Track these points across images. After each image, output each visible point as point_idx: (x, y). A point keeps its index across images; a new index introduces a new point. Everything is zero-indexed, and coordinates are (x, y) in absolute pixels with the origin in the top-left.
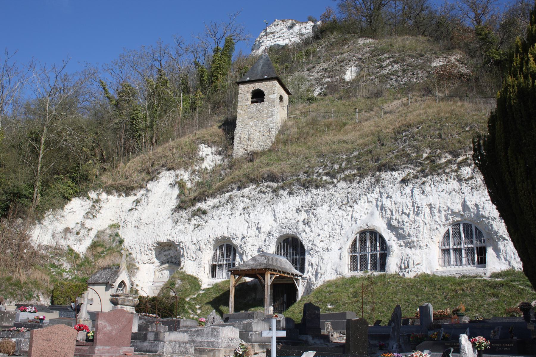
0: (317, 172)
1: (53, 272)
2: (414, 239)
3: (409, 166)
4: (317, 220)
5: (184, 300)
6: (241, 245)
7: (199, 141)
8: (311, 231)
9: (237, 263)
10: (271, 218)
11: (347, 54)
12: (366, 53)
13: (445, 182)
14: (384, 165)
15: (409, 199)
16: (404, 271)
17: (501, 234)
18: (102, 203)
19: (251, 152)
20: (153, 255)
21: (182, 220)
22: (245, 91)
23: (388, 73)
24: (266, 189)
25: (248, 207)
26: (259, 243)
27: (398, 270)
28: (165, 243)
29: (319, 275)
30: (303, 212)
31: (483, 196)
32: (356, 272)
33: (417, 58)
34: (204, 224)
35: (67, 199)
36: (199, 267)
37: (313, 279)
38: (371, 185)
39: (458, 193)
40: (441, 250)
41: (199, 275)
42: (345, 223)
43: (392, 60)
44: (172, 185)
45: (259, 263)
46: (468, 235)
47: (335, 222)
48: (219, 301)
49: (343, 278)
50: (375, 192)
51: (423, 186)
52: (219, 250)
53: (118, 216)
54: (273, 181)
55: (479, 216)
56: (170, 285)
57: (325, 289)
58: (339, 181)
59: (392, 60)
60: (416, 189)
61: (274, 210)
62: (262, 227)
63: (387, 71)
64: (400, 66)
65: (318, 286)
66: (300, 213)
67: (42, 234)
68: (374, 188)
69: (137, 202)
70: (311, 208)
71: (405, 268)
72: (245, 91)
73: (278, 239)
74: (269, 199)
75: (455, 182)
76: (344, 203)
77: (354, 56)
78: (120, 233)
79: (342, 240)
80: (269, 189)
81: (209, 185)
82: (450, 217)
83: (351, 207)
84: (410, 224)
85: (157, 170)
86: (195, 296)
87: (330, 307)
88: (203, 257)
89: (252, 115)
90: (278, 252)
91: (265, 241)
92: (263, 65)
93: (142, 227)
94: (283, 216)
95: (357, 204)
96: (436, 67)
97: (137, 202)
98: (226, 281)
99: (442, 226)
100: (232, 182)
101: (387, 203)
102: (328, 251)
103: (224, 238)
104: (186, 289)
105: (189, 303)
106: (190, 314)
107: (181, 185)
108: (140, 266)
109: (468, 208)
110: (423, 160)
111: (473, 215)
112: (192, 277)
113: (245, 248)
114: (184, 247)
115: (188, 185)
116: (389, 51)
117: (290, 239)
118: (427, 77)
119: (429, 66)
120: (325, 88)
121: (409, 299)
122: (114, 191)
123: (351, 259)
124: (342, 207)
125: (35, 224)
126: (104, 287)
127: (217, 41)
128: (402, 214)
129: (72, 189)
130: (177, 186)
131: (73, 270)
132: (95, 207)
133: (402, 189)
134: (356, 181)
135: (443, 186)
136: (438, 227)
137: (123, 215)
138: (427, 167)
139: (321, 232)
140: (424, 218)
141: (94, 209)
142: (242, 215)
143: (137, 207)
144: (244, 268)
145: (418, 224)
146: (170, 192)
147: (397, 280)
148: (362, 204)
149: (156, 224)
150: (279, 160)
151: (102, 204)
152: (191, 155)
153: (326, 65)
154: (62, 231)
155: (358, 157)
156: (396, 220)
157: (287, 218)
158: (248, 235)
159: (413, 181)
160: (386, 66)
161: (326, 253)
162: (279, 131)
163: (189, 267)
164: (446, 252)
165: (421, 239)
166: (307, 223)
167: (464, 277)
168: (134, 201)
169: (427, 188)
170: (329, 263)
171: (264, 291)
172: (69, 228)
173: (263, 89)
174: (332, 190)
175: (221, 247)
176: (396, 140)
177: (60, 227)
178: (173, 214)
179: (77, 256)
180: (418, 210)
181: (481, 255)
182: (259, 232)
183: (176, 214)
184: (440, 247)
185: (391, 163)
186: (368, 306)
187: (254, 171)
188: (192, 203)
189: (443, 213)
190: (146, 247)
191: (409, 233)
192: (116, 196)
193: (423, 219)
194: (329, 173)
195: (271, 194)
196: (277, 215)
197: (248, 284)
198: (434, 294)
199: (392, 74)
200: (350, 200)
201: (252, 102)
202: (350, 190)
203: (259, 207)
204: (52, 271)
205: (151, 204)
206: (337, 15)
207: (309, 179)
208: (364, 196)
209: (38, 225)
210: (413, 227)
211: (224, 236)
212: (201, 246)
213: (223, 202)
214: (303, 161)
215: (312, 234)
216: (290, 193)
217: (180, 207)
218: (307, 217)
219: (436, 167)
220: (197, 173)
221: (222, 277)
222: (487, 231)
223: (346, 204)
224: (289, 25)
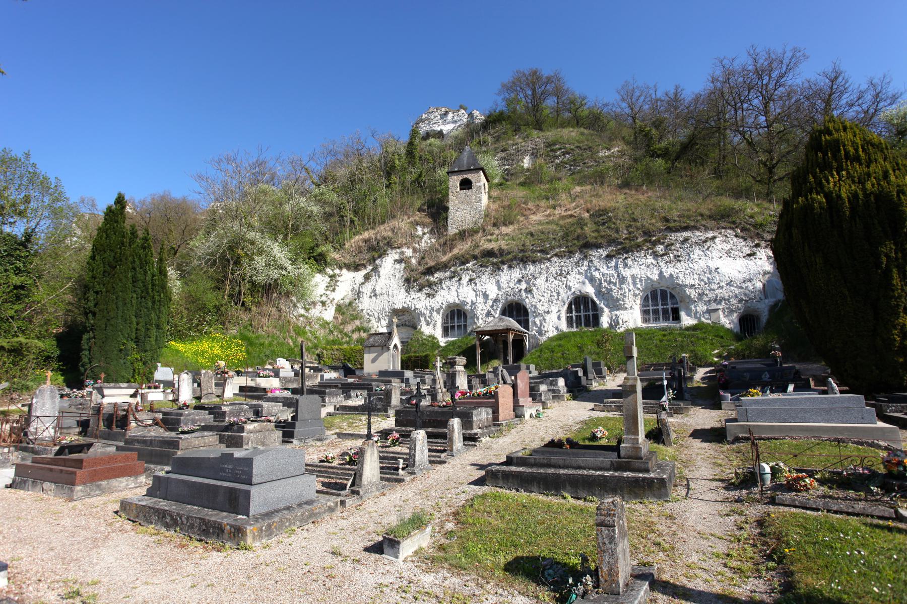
22: (455, 182)
36: (433, 329)
42: (561, 291)
73: (504, 305)
101: (596, 274)
103: (455, 305)
169: (629, 262)
203: (484, 278)
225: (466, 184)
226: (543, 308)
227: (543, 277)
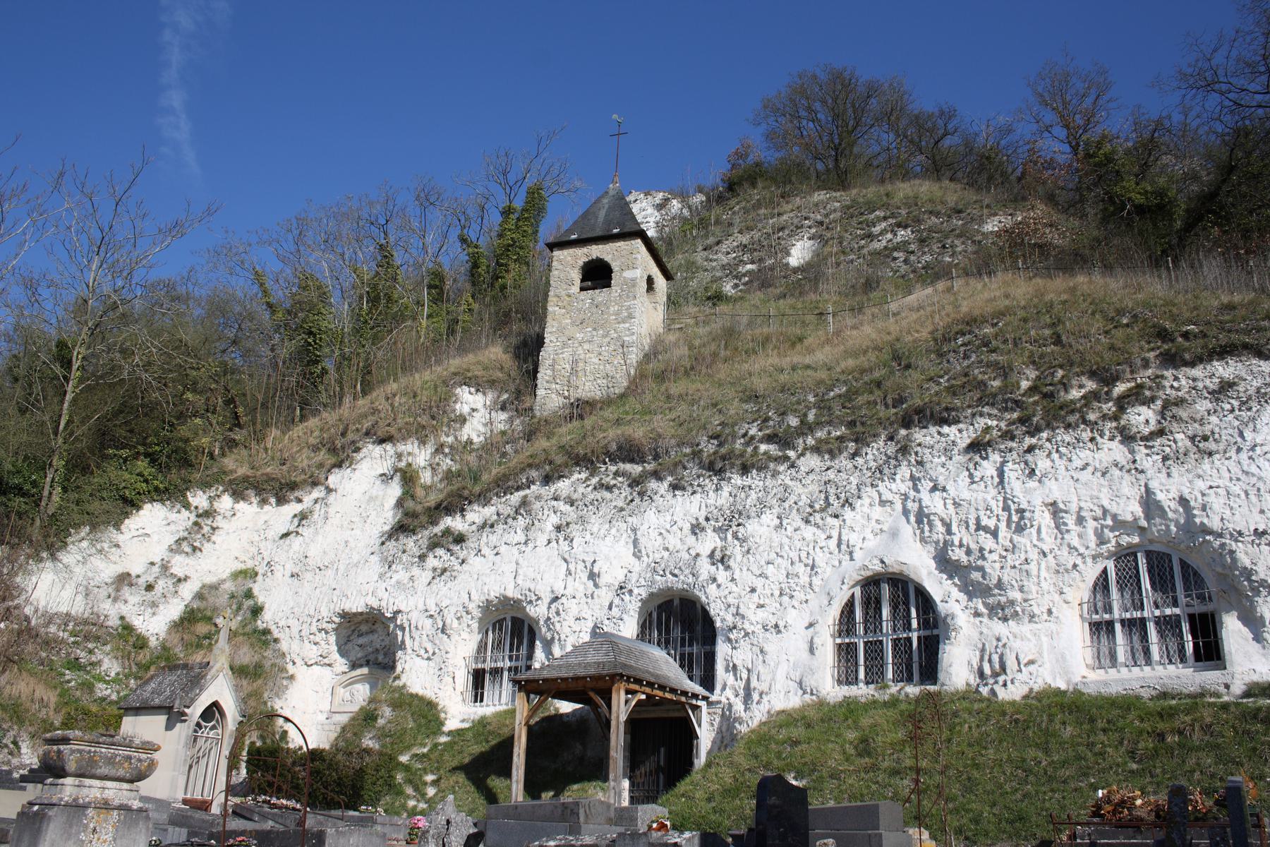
0: (745, 435)
1: (69, 681)
2: (1015, 595)
3: (986, 410)
4: (748, 552)
5: (392, 758)
6: (549, 619)
7: (457, 379)
8: (733, 580)
9: (537, 665)
12: (835, 211)
13: (1089, 445)
14: (919, 411)
15: (993, 492)
16: (991, 681)
17: (1262, 576)
18: (219, 518)
19: (578, 400)
20: (330, 645)
21: (404, 557)
22: (568, 264)
23: (886, 247)
24: (614, 478)
25: (568, 524)
26: (594, 612)
27: (974, 680)
28: (361, 614)
29: (756, 697)
30: (709, 531)
31: (1199, 476)
32: (854, 688)
33: (949, 217)
34: (457, 567)
35: (130, 504)
36: (443, 676)
37: (739, 706)
38: (886, 462)
39: (1129, 471)
40: (1087, 625)
41: (441, 694)
42: (821, 558)
43: (892, 221)
44: (385, 478)
45: (595, 660)
46: (1162, 581)
47: (794, 555)
48: (484, 763)
49: (821, 704)
50: (898, 477)
51: (1029, 457)
52: (494, 631)
53: (255, 550)
54: (632, 461)
55: (1193, 530)
56: (367, 717)
57: (773, 732)
58: (803, 454)
59: (892, 221)
60: (1010, 464)
61: (634, 530)
62: (603, 571)
63: (884, 243)
65: (754, 724)
67: (54, 588)
68: (895, 467)
69: (303, 517)
70: (730, 523)
71: (995, 675)
74: (620, 504)
75: (1115, 445)
76: (817, 507)
78: (256, 592)
79: (814, 603)
80: (620, 479)
81: (476, 479)
82: (1111, 535)
83: (836, 516)
84: (1001, 557)
85: (353, 442)
86: (425, 750)
88: (451, 649)
90: (643, 634)
91: (610, 608)
93: (308, 576)
94: (657, 544)
95: (853, 509)
97: (303, 517)
98: (506, 712)
99: (1089, 560)
100: (530, 466)
101: (934, 503)
102: (779, 632)
103: (505, 602)
104: (405, 730)
105: (407, 768)
106: (408, 797)
107: (408, 477)
108: (298, 670)
109: (1161, 509)
110: (1023, 395)
111: (1173, 529)
112: (421, 699)
113: (558, 626)
114: (406, 625)
115: (426, 477)
116: (885, 206)
117: (676, 602)
118: (975, 253)
119: (978, 231)
120: (745, 284)
121: (1024, 760)
122: (251, 493)
124: (811, 519)
125: (41, 560)
126: (162, 719)
127: (508, 190)
128: (977, 530)
129: (146, 481)
130: (397, 478)
131: (127, 676)
132: (201, 528)
133: (971, 466)
134: (845, 454)
135: (1084, 455)
136: (1079, 561)
137: (268, 549)
138: (1035, 410)
139: (758, 583)
140: (1039, 539)
141: (198, 532)
142: (554, 544)
143: (300, 530)
144: (554, 674)
145: (1023, 557)
146: (381, 493)
147: (976, 706)
148: (866, 509)
149: (342, 568)
150: (647, 411)
151: (219, 521)
152: (435, 409)
154: (109, 581)
155: (848, 397)
156: (961, 545)
158: (566, 592)
159: (1003, 447)
160: (881, 234)
161: (771, 636)
162: (646, 355)
163: (415, 674)
164: (1101, 629)
165: (1035, 595)
166: (721, 559)
167: (1164, 695)
168: (295, 516)
170: (782, 662)
171: (608, 739)
172: (129, 574)
173: (608, 258)
174: (785, 477)
175: (498, 625)
176: (941, 355)
177: (106, 570)
178: (383, 543)
179: (141, 643)
180: (1022, 518)
181: (1206, 634)
182: (596, 585)
183: (391, 544)
184: (1086, 615)
185: (939, 404)
186: (906, 782)
187: (584, 437)
188: (430, 517)
189: (1091, 525)
190: (314, 624)
191: (1000, 580)
192: (255, 505)
193: (1035, 542)
194: (776, 435)
195: (626, 491)
196: (643, 541)
197: (566, 719)
198: (1093, 744)
199: (895, 249)
201: (582, 289)
202: (831, 475)
203: (596, 523)
204: (67, 677)
205: (335, 520)
206: (761, 152)
207: (723, 450)
208: (869, 489)
209: (49, 564)
210: (1010, 563)
211: (505, 597)
212: (448, 621)
213: (506, 514)
214: (707, 413)
215: (734, 588)
216: (675, 487)
217: (401, 529)
218: (719, 544)
219: (1061, 408)
220: (447, 450)
221: (501, 700)
222: (1219, 569)
223: (823, 510)
225: (597, 275)
226: (761, 615)
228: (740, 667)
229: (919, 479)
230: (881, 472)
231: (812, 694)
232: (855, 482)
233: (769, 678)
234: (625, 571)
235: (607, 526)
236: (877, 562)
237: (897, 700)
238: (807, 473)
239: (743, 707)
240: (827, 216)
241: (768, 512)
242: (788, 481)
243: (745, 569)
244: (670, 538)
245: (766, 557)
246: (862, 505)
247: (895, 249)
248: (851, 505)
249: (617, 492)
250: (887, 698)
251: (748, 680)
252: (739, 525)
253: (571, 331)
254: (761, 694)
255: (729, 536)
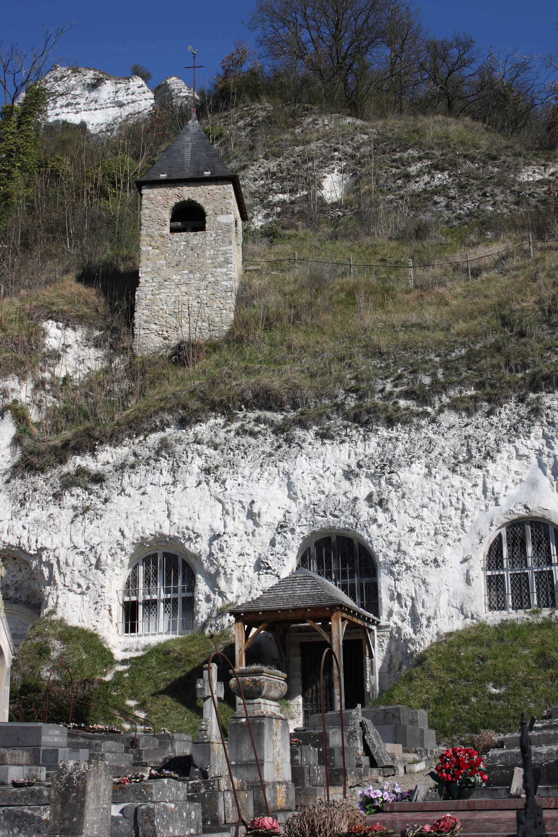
4: (403, 497)
6: (211, 554)
8: (392, 520)
10: (282, 494)
11: (319, 143)
21: (37, 495)
23: (425, 191)
24: (256, 425)
25: (217, 467)
29: (424, 621)
33: (485, 163)
37: (407, 630)
41: (99, 626)
42: (469, 503)
47: (445, 500)
50: (532, 435)
54: (270, 409)
58: (441, 411)
61: (287, 474)
62: (263, 511)
64: (450, 176)
66: (355, 481)
68: (529, 426)
70: (384, 468)
72: (158, 204)
74: (268, 450)
76: (461, 458)
77: (335, 150)
80: (262, 426)
83: (480, 467)
87: (494, 691)
88: (107, 584)
89: (177, 258)
92: (194, 146)
94: (312, 487)
96: (528, 183)
100: (162, 409)
102: (438, 566)
103: (160, 538)
114: (54, 562)
115: (34, 416)
116: (419, 145)
117: (334, 539)
120: (279, 215)
123: (489, 587)
124: (458, 468)
134: (480, 412)
139: (416, 524)
142: (204, 485)
148: (504, 462)
153: (272, 165)
157: (323, 492)
161: (431, 569)
174: (429, 431)
175: (149, 560)
178: (8, 482)
182: (256, 524)
183: (17, 482)
194: (413, 392)
195: (271, 438)
196: (298, 485)
200: (474, 452)
202: (470, 430)
203: (246, 467)
206: (257, 60)
208: (506, 444)
211: (162, 535)
212: (103, 558)
218: (373, 489)
220: (48, 387)
223: (465, 462)
224: (89, 81)
225: (189, 217)
226: (419, 551)
227: (418, 467)
228: (404, 596)
229: (552, 438)
230: (516, 430)
231: (472, 618)
232: (493, 438)
233: (433, 605)
234: (283, 512)
235: (259, 470)
236: (520, 507)
237: (551, 623)
238: (449, 428)
239: (411, 631)
240: (358, 148)
241: (417, 462)
242: (431, 435)
243: (402, 511)
244: (324, 482)
245: (419, 502)
246: (502, 457)
247: (435, 192)
248: (492, 458)
249: (260, 436)
250: (540, 620)
251: (413, 606)
252: (392, 472)
253: (167, 272)
254: (428, 619)
255: (383, 482)
